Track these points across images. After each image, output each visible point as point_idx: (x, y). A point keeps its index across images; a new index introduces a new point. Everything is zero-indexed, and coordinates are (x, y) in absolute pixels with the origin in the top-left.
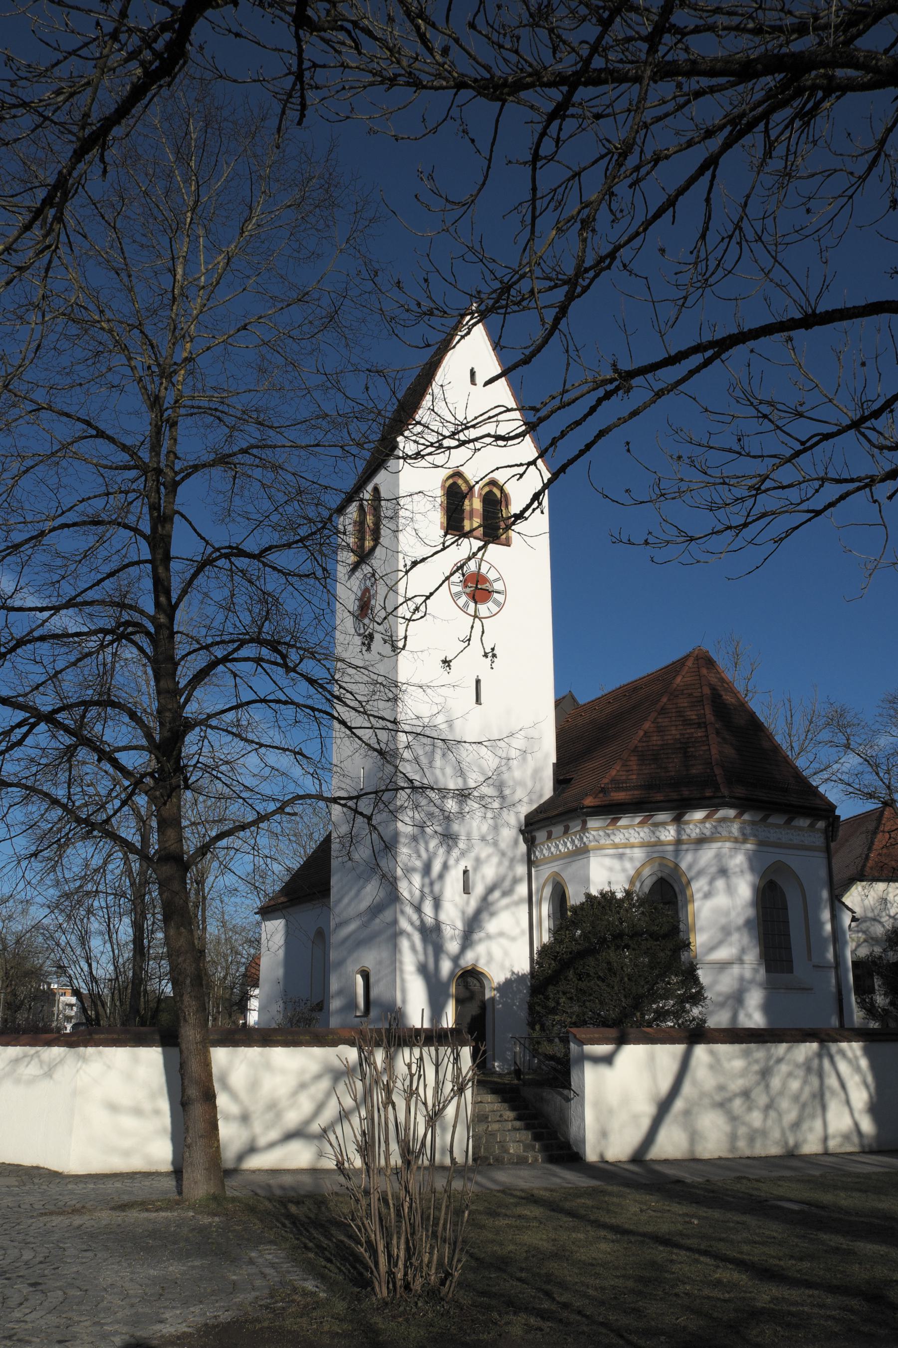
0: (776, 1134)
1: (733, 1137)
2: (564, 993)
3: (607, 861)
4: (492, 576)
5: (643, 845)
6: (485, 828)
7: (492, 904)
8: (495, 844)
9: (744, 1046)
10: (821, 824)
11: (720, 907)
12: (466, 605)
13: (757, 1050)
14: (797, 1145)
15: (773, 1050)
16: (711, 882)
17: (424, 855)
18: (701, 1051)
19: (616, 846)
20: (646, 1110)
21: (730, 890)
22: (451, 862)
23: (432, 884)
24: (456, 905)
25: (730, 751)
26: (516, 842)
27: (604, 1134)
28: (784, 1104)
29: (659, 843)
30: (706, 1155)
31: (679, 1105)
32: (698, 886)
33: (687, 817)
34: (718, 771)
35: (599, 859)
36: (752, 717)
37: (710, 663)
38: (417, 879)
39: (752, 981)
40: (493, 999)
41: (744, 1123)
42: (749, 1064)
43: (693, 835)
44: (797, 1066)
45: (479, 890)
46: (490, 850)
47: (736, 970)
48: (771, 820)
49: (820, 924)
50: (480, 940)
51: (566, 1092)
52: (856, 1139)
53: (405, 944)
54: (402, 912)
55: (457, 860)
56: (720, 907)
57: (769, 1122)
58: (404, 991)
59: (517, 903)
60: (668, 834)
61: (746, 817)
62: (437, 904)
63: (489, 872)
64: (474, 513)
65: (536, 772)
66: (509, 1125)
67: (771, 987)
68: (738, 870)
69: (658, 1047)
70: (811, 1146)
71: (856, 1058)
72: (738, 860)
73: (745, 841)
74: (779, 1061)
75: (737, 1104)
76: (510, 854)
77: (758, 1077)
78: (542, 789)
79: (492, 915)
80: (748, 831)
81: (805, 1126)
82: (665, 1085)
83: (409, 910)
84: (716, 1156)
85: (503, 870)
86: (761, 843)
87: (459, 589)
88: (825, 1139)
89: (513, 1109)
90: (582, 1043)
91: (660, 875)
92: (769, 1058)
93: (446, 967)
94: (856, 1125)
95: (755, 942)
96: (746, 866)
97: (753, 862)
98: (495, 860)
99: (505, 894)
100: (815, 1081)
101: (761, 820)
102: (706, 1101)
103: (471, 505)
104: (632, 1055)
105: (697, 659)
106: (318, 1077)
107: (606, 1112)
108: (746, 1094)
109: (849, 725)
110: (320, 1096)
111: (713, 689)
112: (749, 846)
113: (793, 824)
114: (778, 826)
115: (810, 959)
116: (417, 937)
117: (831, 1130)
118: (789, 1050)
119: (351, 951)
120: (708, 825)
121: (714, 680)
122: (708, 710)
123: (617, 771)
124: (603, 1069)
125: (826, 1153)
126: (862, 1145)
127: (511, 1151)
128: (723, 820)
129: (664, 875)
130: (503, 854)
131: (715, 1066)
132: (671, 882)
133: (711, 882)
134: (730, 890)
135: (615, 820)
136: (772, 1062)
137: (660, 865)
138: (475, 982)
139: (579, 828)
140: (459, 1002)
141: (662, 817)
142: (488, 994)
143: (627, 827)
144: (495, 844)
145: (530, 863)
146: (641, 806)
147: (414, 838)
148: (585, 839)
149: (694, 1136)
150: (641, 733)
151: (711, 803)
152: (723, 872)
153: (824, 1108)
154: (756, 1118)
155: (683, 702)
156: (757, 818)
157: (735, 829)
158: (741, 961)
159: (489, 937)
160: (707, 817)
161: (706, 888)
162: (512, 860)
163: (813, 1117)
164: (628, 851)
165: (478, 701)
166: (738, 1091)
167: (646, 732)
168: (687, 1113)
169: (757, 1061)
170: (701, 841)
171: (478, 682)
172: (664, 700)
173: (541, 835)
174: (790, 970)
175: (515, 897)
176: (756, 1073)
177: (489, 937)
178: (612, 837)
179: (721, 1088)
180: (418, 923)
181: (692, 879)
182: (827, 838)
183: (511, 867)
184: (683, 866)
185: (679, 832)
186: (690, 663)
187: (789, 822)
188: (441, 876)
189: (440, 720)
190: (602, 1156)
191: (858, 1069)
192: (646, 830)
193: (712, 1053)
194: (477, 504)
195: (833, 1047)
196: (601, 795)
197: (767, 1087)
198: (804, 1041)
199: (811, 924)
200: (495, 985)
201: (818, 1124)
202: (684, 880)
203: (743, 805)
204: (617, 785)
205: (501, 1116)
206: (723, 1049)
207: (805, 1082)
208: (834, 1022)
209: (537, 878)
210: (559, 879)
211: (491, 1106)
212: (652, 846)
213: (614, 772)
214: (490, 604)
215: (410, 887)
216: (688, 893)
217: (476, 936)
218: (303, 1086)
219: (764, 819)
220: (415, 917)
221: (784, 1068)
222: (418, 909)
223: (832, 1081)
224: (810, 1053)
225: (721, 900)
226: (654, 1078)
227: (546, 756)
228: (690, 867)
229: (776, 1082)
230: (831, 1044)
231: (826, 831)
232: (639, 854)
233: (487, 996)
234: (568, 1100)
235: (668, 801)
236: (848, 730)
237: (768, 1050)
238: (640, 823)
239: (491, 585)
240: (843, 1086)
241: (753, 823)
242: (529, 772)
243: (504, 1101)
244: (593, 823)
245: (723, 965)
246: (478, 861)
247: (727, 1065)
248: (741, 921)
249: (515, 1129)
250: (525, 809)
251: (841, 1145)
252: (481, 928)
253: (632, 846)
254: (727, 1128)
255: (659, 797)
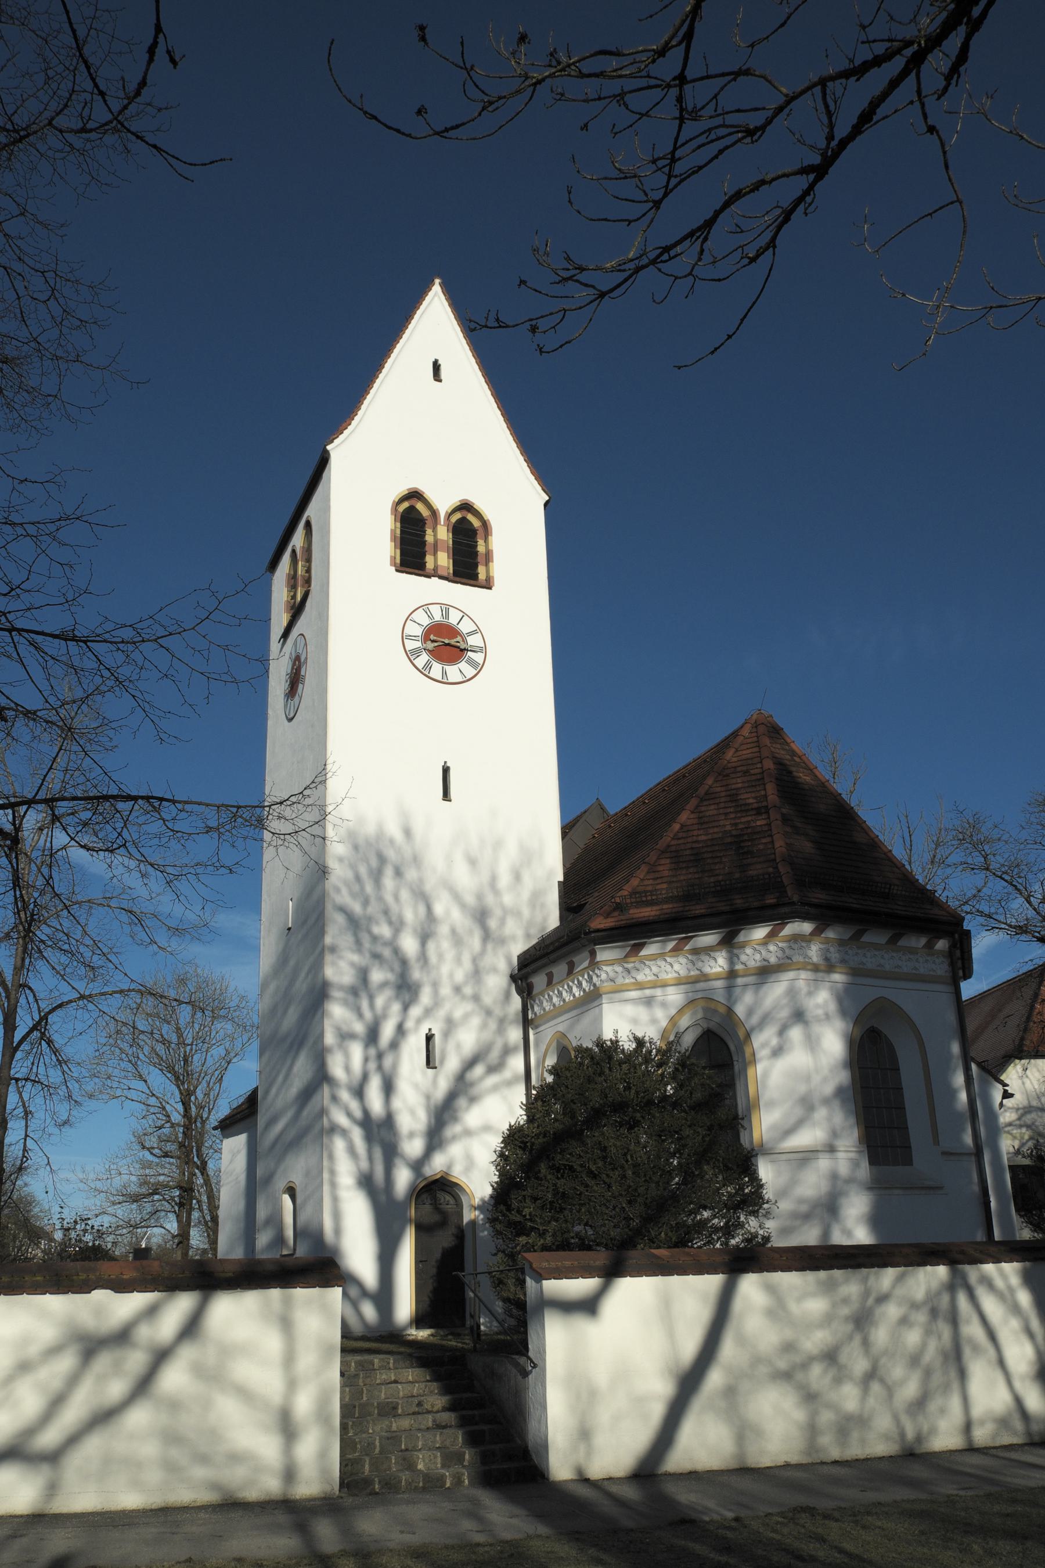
0: (883, 1422)
1: (812, 1430)
2: (535, 1199)
3: (630, 1010)
4: (465, 627)
5: (679, 982)
6: (460, 976)
7: (472, 1084)
8: (476, 998)
9: (822, 1274)
10: (942, 944)
11: (797, 1066)
12: (428, 666)
13: (847, 1281)
14: (919, 1439)
15: (872, 1281)
16: (782, 1032)
17: (368, 1015)
18: (751, 1288)
19: (640, 986)
20: (660, 1389)
21: (812, 1043)
22: (409, 1024)
23: (380, 1056)
24: (416, 1086)
25: (806, 846)
26: (507, 996)
27: (584, 1434)
28: (897, 1371)
29: (704, 977)
30: (766, 1462)
31: (715, 1379)
32: (763, 1040)
33: (741, 937)
34: (783, 869)
35: (617, 1006)
36: (836, 798)
37: (775, 732)
38: (357, 1051)
39: (849, 1181)
40: (473, 1223)
41: (829, 1406)
42: (834, 1305)
43: (752, 964)
44: (914, 1306)
45: (452, 1064)
46: (468, 1007)
47: (824, 1163)
48: (867, 938)
49: (953, 1093)
50: (454, 1138)
51: (522, 1360)
52: (1018, 1425)
53: (339, 1145)
54: (334, 1098)
55: (419, 1021)
56: (797, 1066)
57: (871, 1401)
58: (337, 1216)
59: (509, 1083)
60: (718, 964)
61: (830, 934)
62: (388, 1088)
63: (468, 1038)
64: (438, 541)
65: (536, 898)
66: (429, 1421)
67: (878, 1186)
68: (820, 1012)
69: (675, 1279)
70: (945, 1438)
71: (1011, 1290)
72: (822, 999)
73: (830, 968)
74: (883, 1299)
75: (817, 1375)
76: (498, 1012)
77: (850, 1327)
78: (545, 920)
79: (473, 1100)
80: (835, 956)
81: (933, 1406)
82: (689, 1347)
83: (345, 1096)
84: (781, 1460)
85: (487, 1035)
86: (855, 972)
87: (419, 644)
88: (968, 1427)
89: (446, 1390)
90: (539, 1277)
91: (705, 1026)
92: (866, 1294)
93: (403, 1178)
94: (1018, 1401)
95: (852, 1120)
96: (832, 1007)
97: (844, 1000)
98: (476, 1021)
99: (492, 1070)
100: (945, 1331)
101: (851, 938)
102: (763, 1370)
103: (435, 536)
104: (634, 1295)
105: (756, 725)
106: (53, 1351)
107: (586, 1397)
108: (830, 1356)
109: (987, 841)
110: (57, 1384)
111: (780, 764)
112: (838, 977)
113: (900, 943)
114: (876, 947)
115: (936, 1141)
116: (357, 1135)
117: (978, 1410)
118: (900, 1279)
119: (280, 1160)
120: (772, 947)
121: (782, 754)
122: (771, 789)
123: (646, 882)
124: (581, 1324)
125: (971, 1449)
126: (1029, 1433)
127: (421, 1466)
128: (796, 938)
129: (712, 1026)
130: (488, 1013)
131: (778, 1311)
132: (723, 1035)
133: (782, 1032)
134: (812, 1043)
135: (638, 948)
136: (870, 1301)
137: (706, 1010)
138: (448, 1198)
139: (586, 964)
140: (421, 1229)
141: (708, 939)
142: (469, 1215)
143: (653, 958)
144: (476, 998)
145: (526, 1023)
146: (676, 924)
147: (354, 991)
148: (595, 979)
149: (744, 1431)
150: (676, 827)
151: (775, 914)
152: (799, 1016)
153: (962, 1374)
154: (849, 1397)
155: (738, 782)
156: (847, 936)
157: (814, 952)
158: (831, 1149)
159: (468, 1133)
160: (772, 935)
161: (774, 1041)
162: (502, 1022)
163: (946, 1388)
164: (658, 992)
165: (446, 795)
166: (815, 1351)
167: (682, 826)
168: (730, 1392)
169: (845, 1301)
170: (765, 972)
171: (446, 771)
172: (710, 781)
173: (539, 981)
174: (908, 1161)
175: (507, 1074)
176: (847, 1319)
177: (468, 1133)
178: (634, 973)
179: (788, 1347)
180: (358, 1114)
181: (753, 1029)
182: (952, 964)
183: (501, 1029)
184: (740, 1010)
185: (732, 960)
186: (746, 732)
187: (893, 940)
188: (394, 1045)
189: (394, 830)
190: (580, 1471)
191: (1015, 1309)
192: (683, 960)
193: (771, 1289)
194: (443, 534)
195: (973, 1273)
196: (616, 914)
197: (866, 1343)
198: (923, 1264)
199: (935, 1092)
200: (477, 1202)
201: (955, 1403)
202: (741, 1034)
203: (824, 916)
204: (641, 898)
205: (420, 1404)
206: (789, 1280)
207: (928, 1332)
208: (980, 1236)
209: (537, 1045)
210: (565, 1043)
211: (409, 1387)
212: (695, 981)
213: (635, 882)
214: (463, 665)
215: (347, 1062)
216: (748, 1051)
217: (452, 1130)
218: (24, 1367)
219: (856, 937)
220: (354, 1106)
221: (892, 1311)
222: (359, 1092)
223: (973, 1330)
224: (935, 1285)
225: (798, 1058)
226: (671, 1334)
227: (551, 873)
228: (750, 1012)
229: (881, 1335)
230: (967, 1268)
231: (950, 954)
232: (675, 997)
233: (466, 1220)
234: (525, 1374)
235: (711, 915)
236: (986, 847)
237: (865, 1280)
238: (673, 950)
239: (465, 641)
240: (992, 1336)
241: (841, 943)
242: (526, 895)
243: (436, 1378)
244: (605, 954)
245: (805, 1157)
246: (450, 1026)
247: (794, 1307)
248: (829, 1089)
249: (439, 1427)
250: (518, 948)
251: (994, 1436)
252: (455, 1119)
253: (664, 985)
254: (799, 1415)
255: (699, 909)
